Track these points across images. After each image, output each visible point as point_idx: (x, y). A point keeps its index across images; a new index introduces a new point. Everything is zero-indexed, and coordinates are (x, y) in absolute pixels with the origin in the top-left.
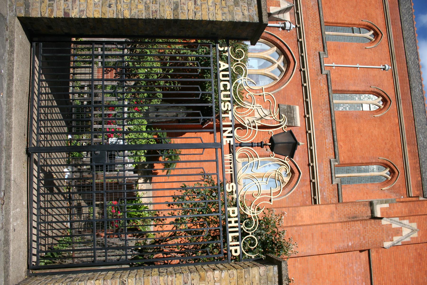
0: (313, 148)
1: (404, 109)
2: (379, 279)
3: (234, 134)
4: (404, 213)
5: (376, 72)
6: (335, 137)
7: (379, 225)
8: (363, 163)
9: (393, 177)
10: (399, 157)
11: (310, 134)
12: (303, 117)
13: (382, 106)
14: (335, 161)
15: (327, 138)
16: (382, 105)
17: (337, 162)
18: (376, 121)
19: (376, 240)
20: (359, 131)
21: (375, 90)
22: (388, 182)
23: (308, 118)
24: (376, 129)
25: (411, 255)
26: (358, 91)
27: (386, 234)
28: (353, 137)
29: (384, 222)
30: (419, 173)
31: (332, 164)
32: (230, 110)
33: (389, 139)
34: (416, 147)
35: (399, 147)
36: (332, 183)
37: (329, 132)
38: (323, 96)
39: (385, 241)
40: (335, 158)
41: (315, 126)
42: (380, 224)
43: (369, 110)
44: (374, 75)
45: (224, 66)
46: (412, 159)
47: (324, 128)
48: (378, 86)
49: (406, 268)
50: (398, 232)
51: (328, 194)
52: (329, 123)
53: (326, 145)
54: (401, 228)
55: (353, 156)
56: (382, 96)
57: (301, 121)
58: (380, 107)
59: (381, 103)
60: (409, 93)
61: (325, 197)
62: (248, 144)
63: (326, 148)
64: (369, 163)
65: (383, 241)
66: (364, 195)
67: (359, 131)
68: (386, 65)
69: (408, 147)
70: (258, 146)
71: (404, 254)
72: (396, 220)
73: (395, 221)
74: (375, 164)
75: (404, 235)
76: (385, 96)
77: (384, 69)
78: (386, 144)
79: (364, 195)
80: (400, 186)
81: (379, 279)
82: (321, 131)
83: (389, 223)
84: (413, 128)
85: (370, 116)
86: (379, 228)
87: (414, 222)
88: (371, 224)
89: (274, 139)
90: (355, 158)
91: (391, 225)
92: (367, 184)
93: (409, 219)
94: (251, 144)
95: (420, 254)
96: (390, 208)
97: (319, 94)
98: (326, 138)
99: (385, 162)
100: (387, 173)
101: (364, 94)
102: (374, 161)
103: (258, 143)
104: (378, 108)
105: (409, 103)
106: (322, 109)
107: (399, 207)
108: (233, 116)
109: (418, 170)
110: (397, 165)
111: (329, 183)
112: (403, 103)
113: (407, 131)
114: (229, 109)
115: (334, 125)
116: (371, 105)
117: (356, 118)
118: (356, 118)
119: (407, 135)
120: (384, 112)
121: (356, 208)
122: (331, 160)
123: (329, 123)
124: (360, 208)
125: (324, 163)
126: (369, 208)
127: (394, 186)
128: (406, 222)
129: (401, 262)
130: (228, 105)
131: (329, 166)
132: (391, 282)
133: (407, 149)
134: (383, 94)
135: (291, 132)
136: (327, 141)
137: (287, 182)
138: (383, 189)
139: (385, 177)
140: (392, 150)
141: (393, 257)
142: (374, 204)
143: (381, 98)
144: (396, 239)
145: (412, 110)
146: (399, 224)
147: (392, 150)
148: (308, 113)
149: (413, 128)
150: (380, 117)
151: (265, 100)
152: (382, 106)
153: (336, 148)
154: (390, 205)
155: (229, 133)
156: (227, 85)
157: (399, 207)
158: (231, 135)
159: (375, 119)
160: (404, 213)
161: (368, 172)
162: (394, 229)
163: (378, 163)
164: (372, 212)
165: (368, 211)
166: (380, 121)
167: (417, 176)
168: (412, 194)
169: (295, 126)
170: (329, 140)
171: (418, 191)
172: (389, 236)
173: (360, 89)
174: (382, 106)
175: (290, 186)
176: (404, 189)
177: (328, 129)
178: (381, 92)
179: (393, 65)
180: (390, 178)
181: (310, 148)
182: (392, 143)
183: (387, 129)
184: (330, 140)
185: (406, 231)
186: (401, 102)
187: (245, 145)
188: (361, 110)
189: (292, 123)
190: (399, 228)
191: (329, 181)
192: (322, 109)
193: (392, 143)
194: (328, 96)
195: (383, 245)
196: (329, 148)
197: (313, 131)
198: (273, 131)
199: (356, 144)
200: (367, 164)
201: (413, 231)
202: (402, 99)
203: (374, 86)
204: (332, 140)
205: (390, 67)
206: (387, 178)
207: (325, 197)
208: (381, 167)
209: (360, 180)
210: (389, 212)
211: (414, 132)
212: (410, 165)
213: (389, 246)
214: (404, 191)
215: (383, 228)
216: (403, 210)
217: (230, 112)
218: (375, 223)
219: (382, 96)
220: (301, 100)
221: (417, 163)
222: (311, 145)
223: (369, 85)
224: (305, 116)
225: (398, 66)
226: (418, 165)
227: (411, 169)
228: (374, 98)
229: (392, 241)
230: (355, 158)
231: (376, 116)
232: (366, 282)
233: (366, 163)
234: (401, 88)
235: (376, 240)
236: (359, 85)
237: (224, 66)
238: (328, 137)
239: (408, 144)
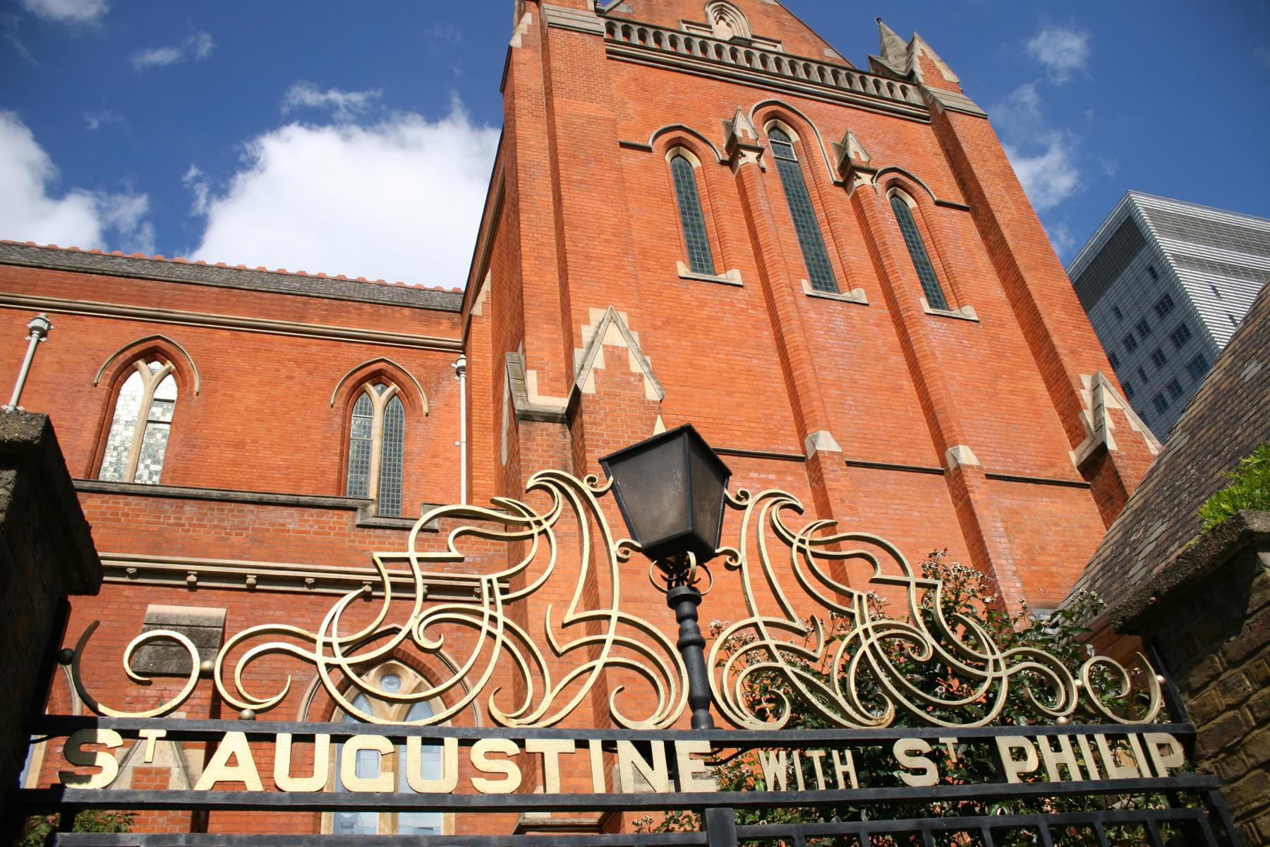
0: (310, 577)
1: (192, 308)
2: (739, 434)
3: (655, 734)
4: (555, 336)
5: (47, 358)
6: (282, 498)
7: (598, 402)
8: (342, 451)
9: (393, 379)
10: (335, 350)
11: (261, 579)
12: (193, 595)
13: (169, 364)
14: (364, 510)
15: (284, 525)
16: (163, 364)
17: (366, 506)
18: (214, 391)
19: (640, 418)
20: (239, 445)
21: (110, 373)
22: (405, 395)
23: (202, 576)
24: (239, 394)
25: (669, 341)
26: (101, 426)
27: (624, 389)
28: (254, 467)
29: (588, 386)
30: (389, 309)
31: (372, 521)
32: (521, 743)
33: (276, 366)
34: (313, 301)
35: (306, 345)
36: (436, 531)
37: (261, 514)
38: (126, 515)
39: (644, 396)
40: (354, 509)
41: (234, 558)
42: (594, 400)
43: (171, 406)
44: (55, 366)
45: (232, 761)
46: (349, 318)
47: (247, 529)
48: (98, 364)
49: (705, 362)
50: (616, 357)
51: (470, 549)
52: (231, 510)
53: (308, 532)
54: (605, 346)
55: (314, 478)
56: (137, 357)
57: (206, 603)
58: (169, 372)
59: (156, 365)
60: (143, 282)
61: (478, 560)
62: (696, 665)
63: (316, 533)
64: (343, 434)
65: (642, 400)
66: (437, 465)
67: (239, 445)
68: (30, 325)
69: (311, 320)
70: (695, 617)
71: (669, 358)
72: (582, 356)
73: (585, 359)
74: (346, 419)
75: (625, 345)
76: (136, 350)
77: (43, 334)
78: (290, 378)
79: (437, 465)
80: (420, 365)
81: (739, 434)
82: (253, 540)
83: (592, 375)
84: (257, 298)
85: (194, 404)
86: (606, 403)
87: (587, 314)
88: (593, 423)
89: (658, 534)
90: (324, 473)
91: (596, 371)
92: (407, 453)
93: (577, 321)
94: (693, 649)
95: (668, 322)
96: (540, 370)
97: (117, 525)
98: (282, 529)
99: (345, 389)
100: (381, 393)
101: (114, 410)
102: (339, 420)
103: (680, 619)
104: (170, 377)
105: (174, 289)
106: (176, 524)
107: (537, 344)
108: (551, 732)
109: (382, 310)
110: (361, 360)
111: (435, 540)
112: (170, 306)
113: (261, 314)
114: (513, 749)
115: (240, 496)
116: (157, 396)
117: (194, 446)
118: (194, 446)
119: (274, 317)
120: (190, 362)
121: (537, 461)
122: (358, 521)
123: (231, 510)
124: (536, 450)
125: (366, 545)
126: (537, 424)
127: (420, 380)
128: (587, 333)
129: (690, 370)
130: (490, 755)
131: (378, 532)
132: (741, 405)
133: (315, 325)
134: (128, 354)
135: (611, 462)
136: (291, 527)
137: (420, 678)
138: (425, 409)
139: (390, 399)
140: (311, 366)
141: (677, 388)
142: (528, 408)
143: (141, 363)
144: (636, 366)
145: (200, 288)
146: (593, 350)
147: (311, 366)
148: (183, 574)
149: (257, 298)
150: (202, 378)
151: (455, 554)
152: (167, 366)
153: (321, 501)
154: (532, 368)
155: (650, 761)
156: (293, 774)
157: (537, 344)
158: (658, 748)
159: (206, 392)
160: (555, 336)
161: (370, 442)
162: (607, 366)
163: (345, 410)
164: (550, 418)
165: (547, 429)
166: (216, 379)
167: (397, 315)
168: (457, 339)
169: (224, 627)
170: (291, 519)
171: (439, 323)
172: (629, 383)
173: (97, 418)
174: (167, 366)
175: (434, 669)
176: (432, 355)
177: (251, 517)
178: (121, 358)
179: (36, 307)
180: (393, 386)
181: (310, 586)
182: (290, 360)
183: (247, 366)
184: (292, 515)
185: (614, 337)
186: (165, 311)
187: (697, 677)
188: (167, 427)
189: (210, 635)
190: (605, 352)
191: (428, 540)
192: (176, 524)
193: (290, 360)
194: (130, 498)
195: (654, 402)
196: (317, 522)
197: (252, 565)
198: (615, 541)
199: (278, 461)
200: (345, 441)
201: (613, 320)
202: (159, 305)
203: (94, 375)
204: (293, 510)
205: (42, 315)
206: (394, 394)
207: (478, 560)
208: (358, 404)
209: (391, 469)
210: (551, 374)
211: (266, 295)
212: (365, 326)
213: (657, 387)
214: (437, 358)
215: (607, 394)
216: (546, 335)
217: (533, 745)
218: (591, 413)
219: (137, 357)
220: (128, 592)
221: (359, 309)
222: (300, 581)
223: (88, 388)
224: (192, 587)
225: (45, 293)
226: (366, 306)
227: (376, 327)
228: (134, 389)
229: (641, 375)
230: (324, 473)
231: (196, 388)
232: (749, 470)
233: (342, 443)
234: (120, 301)
235: (640, 418)
236: (81, 418)
237: (232, 761)
238: (281, 521)
239: (301, 319)
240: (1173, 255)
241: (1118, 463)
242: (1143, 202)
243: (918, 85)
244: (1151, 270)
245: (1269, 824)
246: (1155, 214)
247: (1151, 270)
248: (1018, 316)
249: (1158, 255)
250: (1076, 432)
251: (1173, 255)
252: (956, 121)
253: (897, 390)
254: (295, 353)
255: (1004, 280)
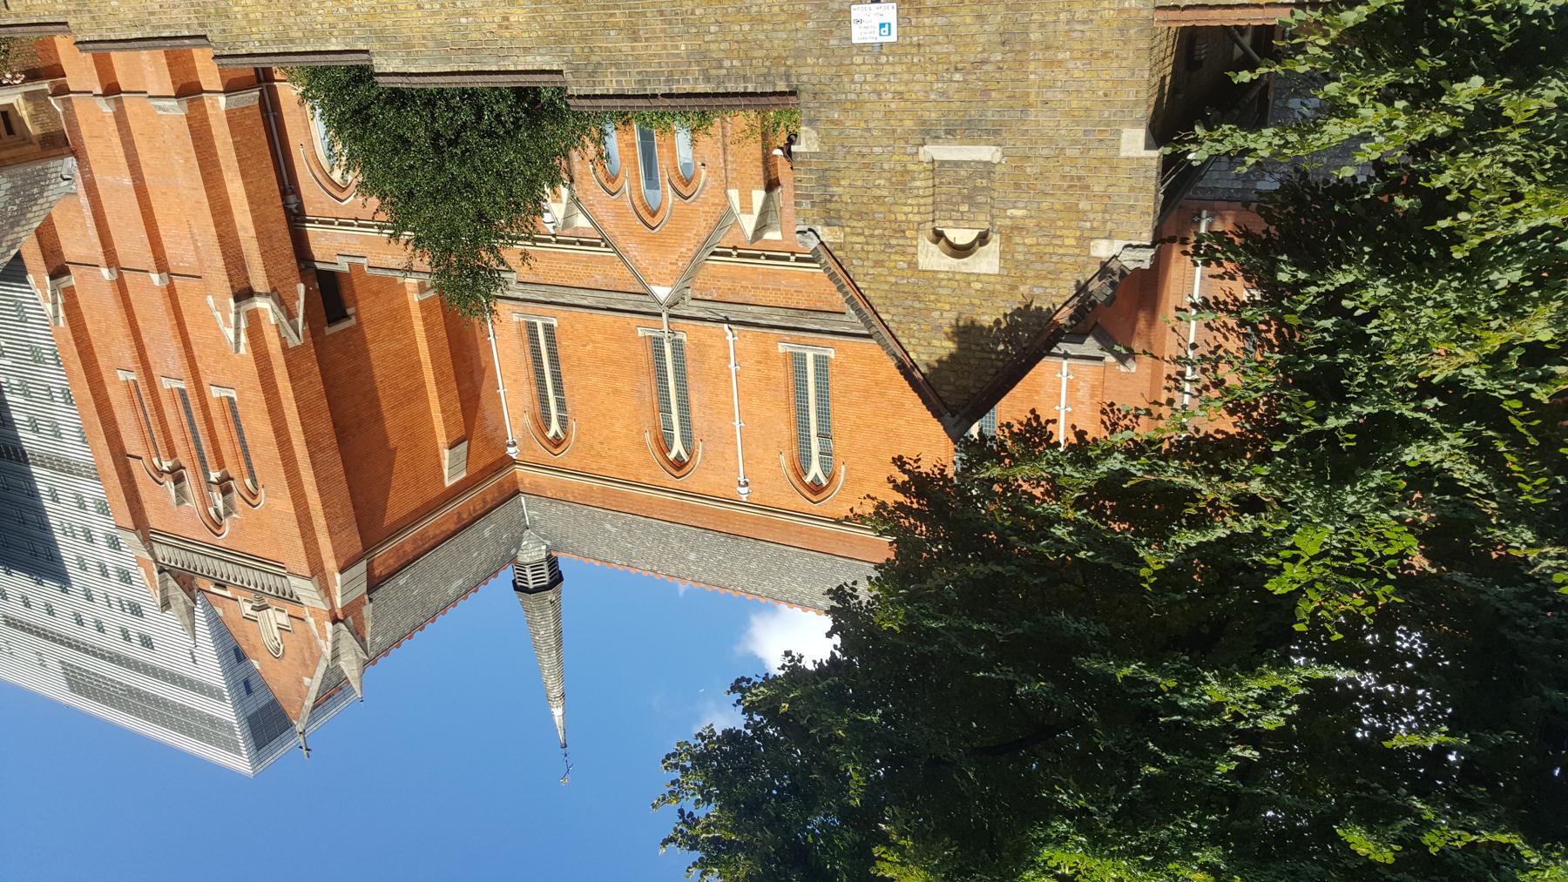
20: (616, 391)
133: (596, 484)
199: (594, 380)
240: (223, 699)
241: (44, 269)
242: (240, 763)
243: (156, 561)
244: (249, 691)
245: (1566, 590)
246: (232, 747)
247: (249, 691)
248: (100, 374)
249: (239, 704)
250: (70, 293)
251: (223, 699)
252: (129, 523)
253: (144, 320)
254: (603, 463)
255: (107, 399)
